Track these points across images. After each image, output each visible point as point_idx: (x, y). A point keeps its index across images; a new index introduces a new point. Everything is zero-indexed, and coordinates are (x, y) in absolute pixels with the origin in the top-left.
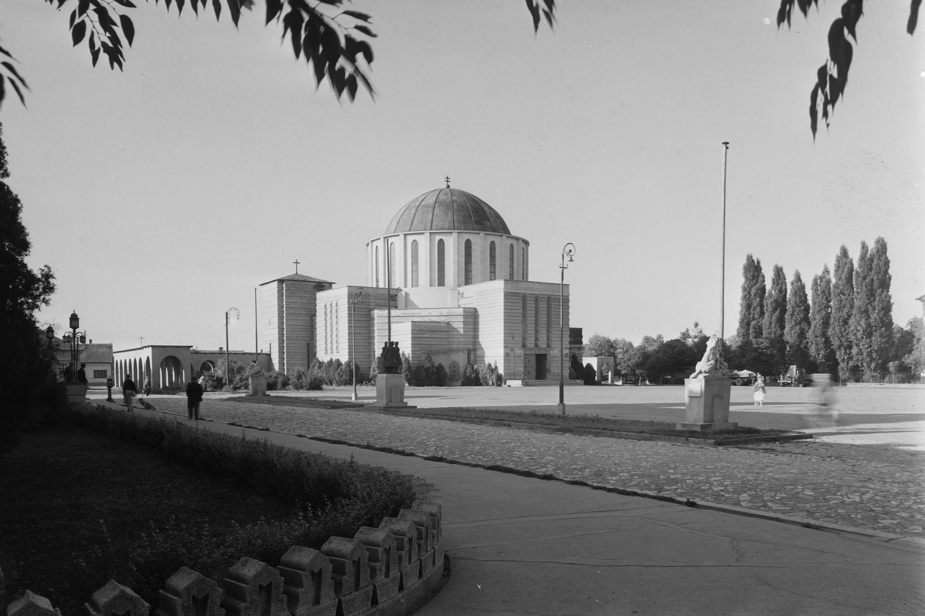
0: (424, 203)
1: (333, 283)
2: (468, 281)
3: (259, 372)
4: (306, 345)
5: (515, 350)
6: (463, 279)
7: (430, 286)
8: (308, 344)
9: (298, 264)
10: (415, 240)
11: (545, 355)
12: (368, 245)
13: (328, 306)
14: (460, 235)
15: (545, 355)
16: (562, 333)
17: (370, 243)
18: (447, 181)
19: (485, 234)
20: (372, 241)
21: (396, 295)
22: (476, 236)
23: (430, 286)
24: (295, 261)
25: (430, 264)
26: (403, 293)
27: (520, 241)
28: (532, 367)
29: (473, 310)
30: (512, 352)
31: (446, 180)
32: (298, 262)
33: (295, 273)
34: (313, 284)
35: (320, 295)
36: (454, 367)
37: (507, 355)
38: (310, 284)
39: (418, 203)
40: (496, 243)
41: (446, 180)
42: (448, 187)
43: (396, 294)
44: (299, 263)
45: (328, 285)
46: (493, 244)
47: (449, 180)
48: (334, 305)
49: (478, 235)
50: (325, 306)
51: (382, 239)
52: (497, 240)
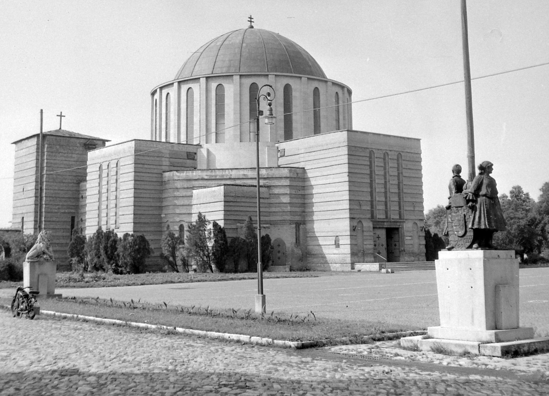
0: (226, 43)
1: (108, 141)
2: (288, 135)
3: (44, 253)
4: (70, 220)
5: (363, 222)
6: (282, 132)
7: (240, 142)
8: (73, 219)
9: (62, 117)
10: (190, 88)
11: (397, 229)
12: (153, 94)
13: (105, 167)
14: (278, 79)
15: (397, 229)
16: (372, 206)
17: (158, 90)
18: (251, 22)
19: (308, 78)
20: (161, 88)
21: (196, 153)
22: (297, 81)
23: (240, 142)
24: (59, 114)
25: (240, 114)
26: (204, 152)
27: (330, 84)
28: (382, 245)
29: (301, 171)
30: (360, 225)
31: (249, 20)
32: (63, 115)
33: (58, 128)
34: (82, 141)
35: (92, 155)
36: (279, 245)
37: (354, 230)
38: (78, 141)
39: (219, 43)
40: (293, 87)
41: (249, 20)
42: (252, 27)
43: (195, 152)
44: (61, 113)
45: (101, 143)
46: (316, 90)
47: (252, 20)
48: (113, 165)
49: (324, 84)
50: (100, 167)
51: (176, 85)
52: (295, 84)
